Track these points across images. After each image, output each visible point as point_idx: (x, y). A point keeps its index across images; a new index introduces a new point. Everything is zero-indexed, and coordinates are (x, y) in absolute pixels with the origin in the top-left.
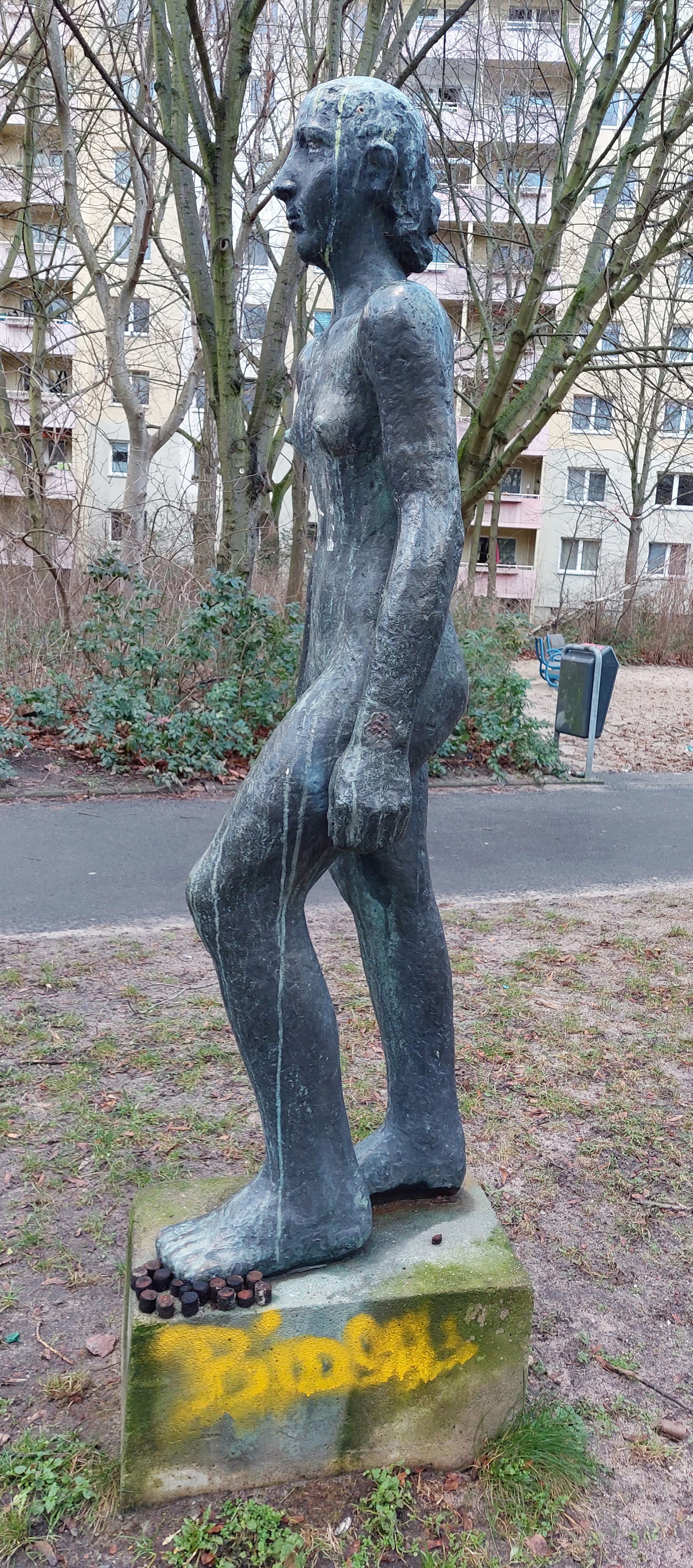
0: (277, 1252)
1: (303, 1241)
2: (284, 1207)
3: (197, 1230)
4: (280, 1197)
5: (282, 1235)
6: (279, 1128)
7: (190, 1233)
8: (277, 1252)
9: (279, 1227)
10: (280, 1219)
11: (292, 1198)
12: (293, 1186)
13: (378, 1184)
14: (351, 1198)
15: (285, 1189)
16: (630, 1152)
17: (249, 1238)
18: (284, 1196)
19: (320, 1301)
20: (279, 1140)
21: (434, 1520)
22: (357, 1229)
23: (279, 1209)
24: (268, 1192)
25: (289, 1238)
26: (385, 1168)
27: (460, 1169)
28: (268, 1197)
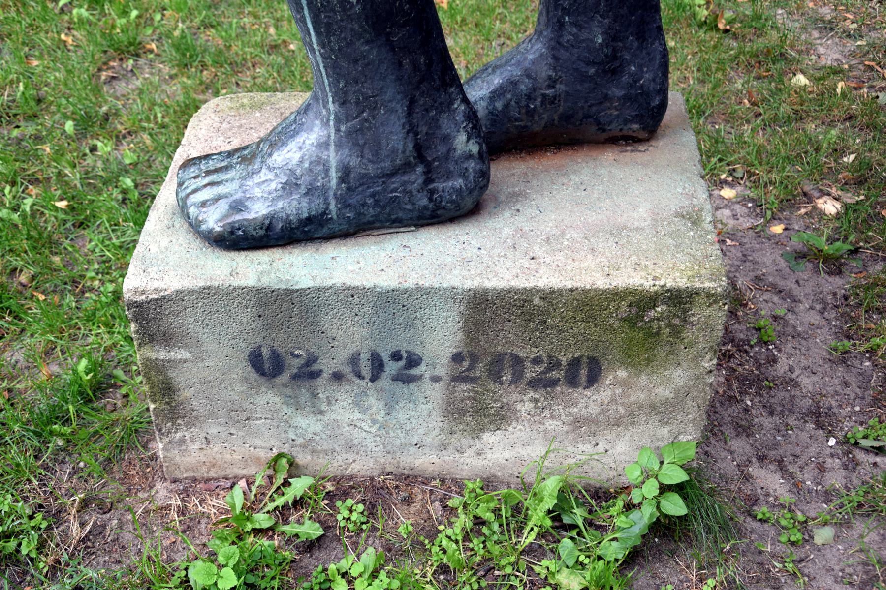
0: (332, 207)
1: (373, 195)
2: (339, 146)
3: (226, 168)
4: (333, 131)
5: (338, 185)
6: (310, 25)
7: (216, 171)
8: (332, 207)
9: (334, 174)
10: (333, 163)
11: (349, 134)
12: (348, 118)
13: (516, 120)
14: (447, 139)
15: (338, 121)
16: (13, 442)
17: (289, 187)
18: (338, 130)
19: (387, 281)
20: (315, 46)
21: (537, 515)
22: (459, 183)
23: (332, 148)
24: (318, 122)
25: (349, 189)
26: (529, 97)
27: (656, 102)
28: (316, 129)
